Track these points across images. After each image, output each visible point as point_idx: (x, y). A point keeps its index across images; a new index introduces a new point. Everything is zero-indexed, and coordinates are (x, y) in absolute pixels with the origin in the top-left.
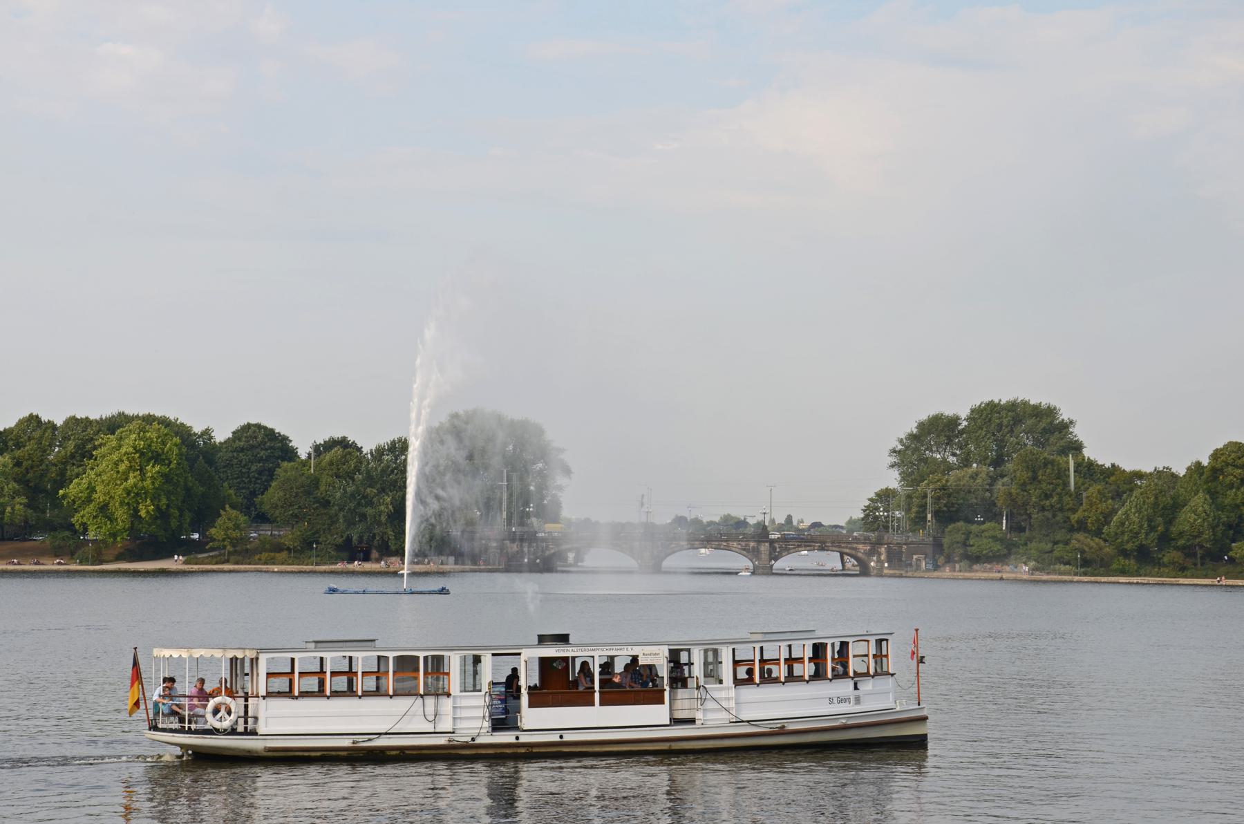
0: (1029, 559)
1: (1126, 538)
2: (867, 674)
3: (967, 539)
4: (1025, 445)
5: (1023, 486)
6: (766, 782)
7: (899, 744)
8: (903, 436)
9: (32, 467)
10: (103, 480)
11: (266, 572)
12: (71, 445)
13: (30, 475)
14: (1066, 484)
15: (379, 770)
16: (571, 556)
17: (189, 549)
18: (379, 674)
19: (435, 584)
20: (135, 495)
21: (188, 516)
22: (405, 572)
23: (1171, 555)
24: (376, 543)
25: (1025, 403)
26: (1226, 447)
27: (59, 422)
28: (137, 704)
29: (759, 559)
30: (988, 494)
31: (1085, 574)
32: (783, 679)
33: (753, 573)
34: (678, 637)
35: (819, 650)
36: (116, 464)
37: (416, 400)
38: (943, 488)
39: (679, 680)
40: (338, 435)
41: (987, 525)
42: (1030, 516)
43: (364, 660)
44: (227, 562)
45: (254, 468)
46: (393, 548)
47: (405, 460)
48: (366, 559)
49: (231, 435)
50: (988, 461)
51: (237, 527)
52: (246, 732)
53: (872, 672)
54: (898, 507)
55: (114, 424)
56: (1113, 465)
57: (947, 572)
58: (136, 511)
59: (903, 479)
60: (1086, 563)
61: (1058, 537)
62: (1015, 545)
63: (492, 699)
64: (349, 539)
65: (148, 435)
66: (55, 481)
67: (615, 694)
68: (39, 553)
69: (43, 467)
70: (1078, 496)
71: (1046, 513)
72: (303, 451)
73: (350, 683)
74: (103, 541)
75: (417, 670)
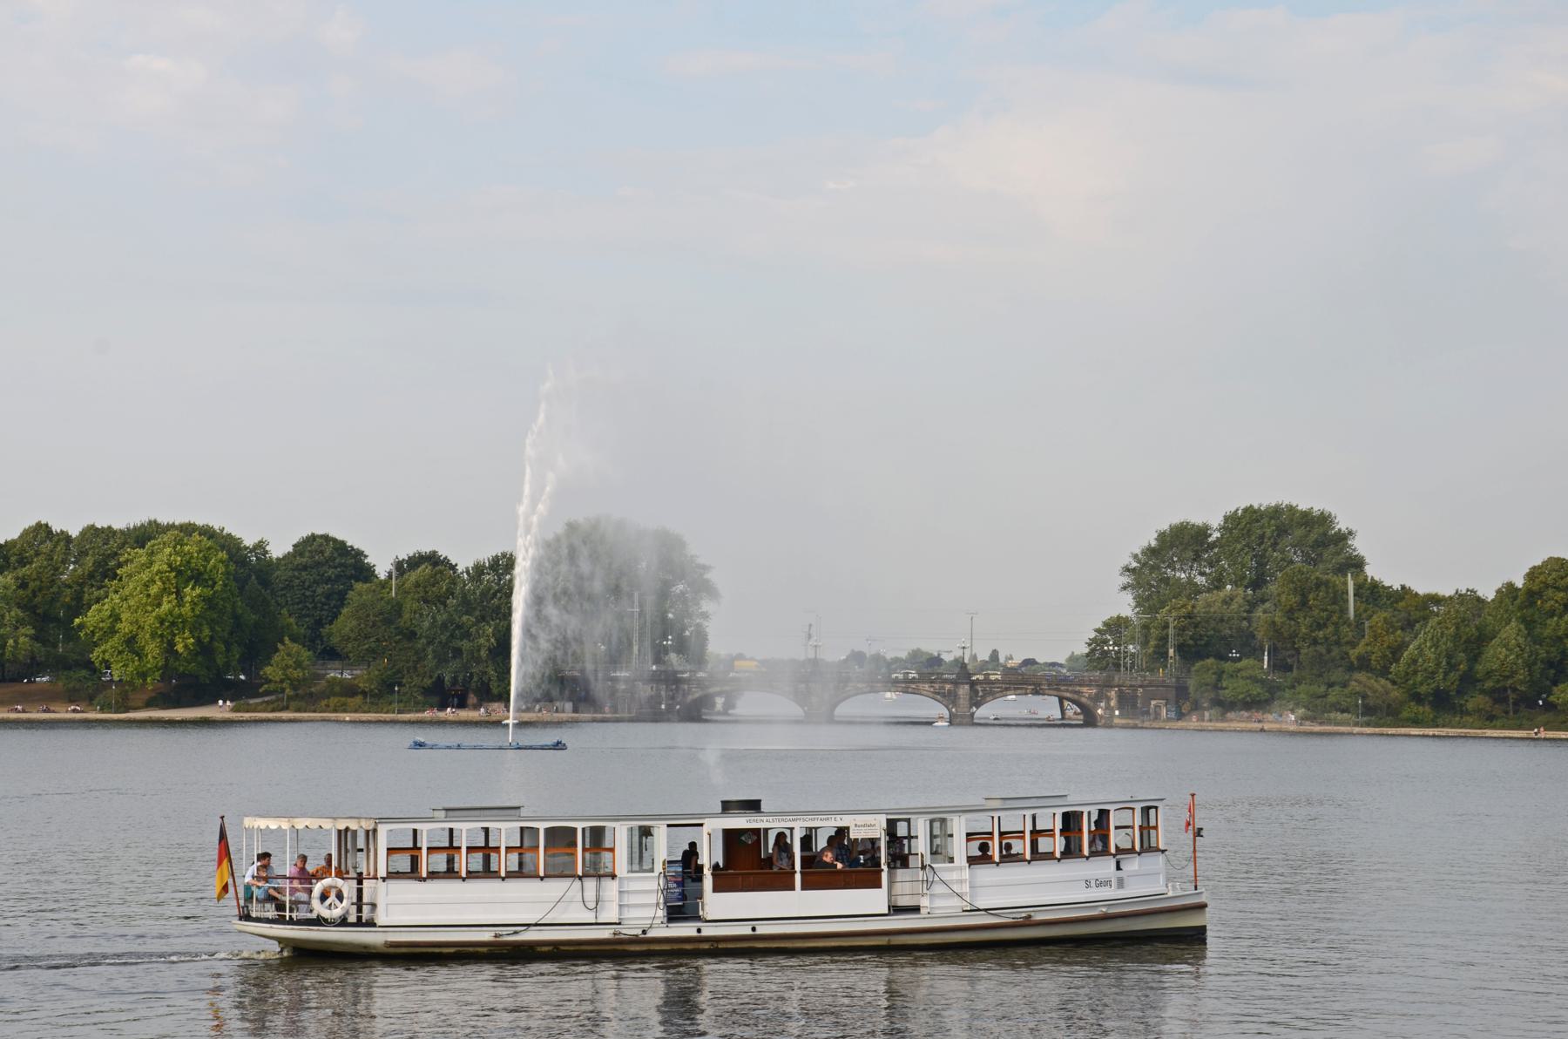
0: (1297, 705)
1: (1419, 678)
2: (1132, 851)
3: (1219, 679)
4: (1292, 562)
5: (1290, 613)
6: (994, 984)
7: (1169, 939)
8: (1138, 551)
9: (40, 589)
10: (130, 607)
11: (337, 721)
12: (89, 561)
13: (38, 599)
14: (1344, 611)
15: (524, 970)
16: (720, 701)
17: (239, 693)
18: (522, 849)
19: (550, 736)
20: (171, 624)
21: (236, 653)
22: (511, 721)
23: (1476, 701)
24: (473, 685)
25: (1291, 509)
26: (1545, 563)
27: (74, 532)
28: (225, 888)
29: (955, 703)
30: (1245, 623)
31: (1368, 725)
32: (1058, 855)
33: (951, 723)
34: (899, 802)
35: (1071, 821)
36: (146, 586)
37: (526, 501)
38: (1189, 616)
39: (900, 859)
40: (426, 549)
41: (1244, 662)
42: (1298, 651)
43: (506, 833)
44: (285, 708)
45: (319, 591)
46: (495, 691)
47: (511, 581)
48: (462, 705)
49: (291, 549)
50: (1246, 582)
51: (298, 665)
52: (359, 923)
53: (1138, 848)
54: (1132, 640)
55: (144, 535)
56: (1403, 587)
57: (1193, 721)
58: (172, 644)
59: (1138, 605)
60: (1369, 710)
61: (1333, 679)
62: (1280, 688)
63: (667, 882)
64: (440, 680)
65: (186, 548)
66: (69, 607)
67: (819, 875)
68: (48, 698)
69: (55, 589)
70: (1359, 625)
71: (1319, 648)
72: (383, 568)
73: (450, 861)
74: (131, 683)
75: (575, 845)
